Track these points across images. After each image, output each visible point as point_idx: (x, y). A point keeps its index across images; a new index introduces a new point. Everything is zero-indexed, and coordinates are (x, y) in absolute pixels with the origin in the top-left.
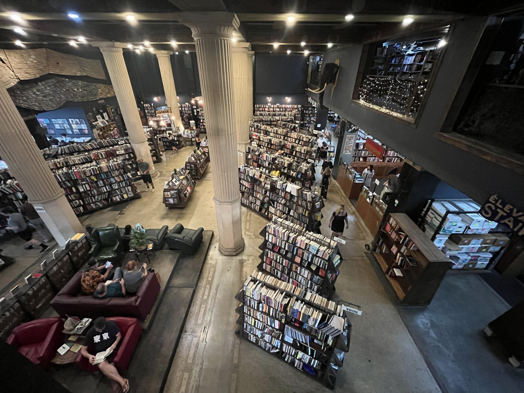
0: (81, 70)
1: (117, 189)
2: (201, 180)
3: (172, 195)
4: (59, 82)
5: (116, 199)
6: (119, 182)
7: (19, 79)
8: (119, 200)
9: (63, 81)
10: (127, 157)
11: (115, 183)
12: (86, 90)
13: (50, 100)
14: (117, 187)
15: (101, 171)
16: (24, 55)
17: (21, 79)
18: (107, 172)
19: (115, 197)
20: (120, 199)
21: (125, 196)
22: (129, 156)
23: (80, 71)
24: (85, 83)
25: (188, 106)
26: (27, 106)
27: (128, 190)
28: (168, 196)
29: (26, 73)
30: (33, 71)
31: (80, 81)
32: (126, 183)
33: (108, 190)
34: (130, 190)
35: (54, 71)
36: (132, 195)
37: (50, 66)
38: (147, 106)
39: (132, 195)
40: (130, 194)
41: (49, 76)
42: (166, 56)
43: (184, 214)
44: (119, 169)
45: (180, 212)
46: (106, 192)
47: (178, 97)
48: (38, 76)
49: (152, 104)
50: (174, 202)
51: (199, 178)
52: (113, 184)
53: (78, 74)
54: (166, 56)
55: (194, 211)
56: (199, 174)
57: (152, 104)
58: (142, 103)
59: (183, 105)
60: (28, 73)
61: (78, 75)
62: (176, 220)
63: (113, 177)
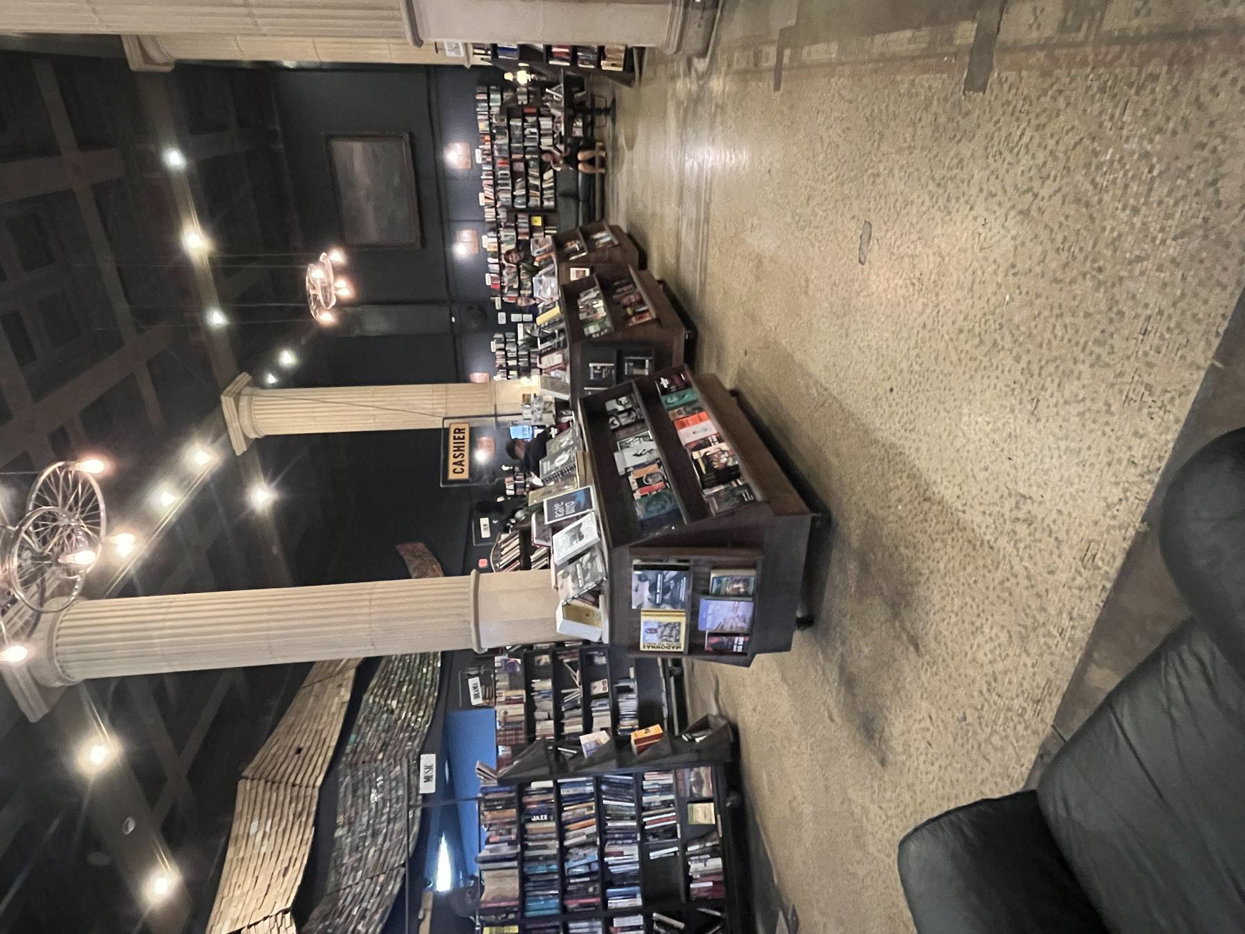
0: (338, 679)
1: (644, 853)
2: (700, 330)
3: (666, 597)
4: (353, 766)
5: (705, 876)
6: (602, 831)
7: (285, 912)
8: (717, 863)
9: (354, 751)
10: (548, 684)
11: (602, 854)
12: (400, 684)
13: (389, 821)
14: (632, 852)
15: (507, 910)
16: (241, 855)
17: (289, 905)
18: (524, 879)
19: (690, 880)
20: (714, 853)
21: (704, 814)
22: (543, 678)
23: (340, 686)
24: (373, 682)
25: (499, 341)
26: (377, 917)
27: (666, 789)
28: (675, 626)
29: (284, 875)
30: (291, 845)
31: (365, 697)
32: (619, 790)
33: (638, 902)
34: (668, 779)
35: (317, 771)
36: (705, 772)
37: (298, 782)
38: (512, 487)
39: (705, 772)
40: (699, 783)
41: (328, 793)
42: (250, 403)
43: (872, 536)
44: (522, 809)
45: (852, 566)
46: (648, 920)
47: (478, 377)
48: (309, 834)
49: (505, 468)
50: (737, 595)
51: (684, 334)
52: (604, 866)
53: (346, 695)
54: (250, 403)
55: (866, 435)
56: (654, 333)
57: (505, 468)
58: (500, 499)
59: (500, 361)
60: (287, 869)
61: (347, 697)
62: (915, 643)
63: (564, 852)
